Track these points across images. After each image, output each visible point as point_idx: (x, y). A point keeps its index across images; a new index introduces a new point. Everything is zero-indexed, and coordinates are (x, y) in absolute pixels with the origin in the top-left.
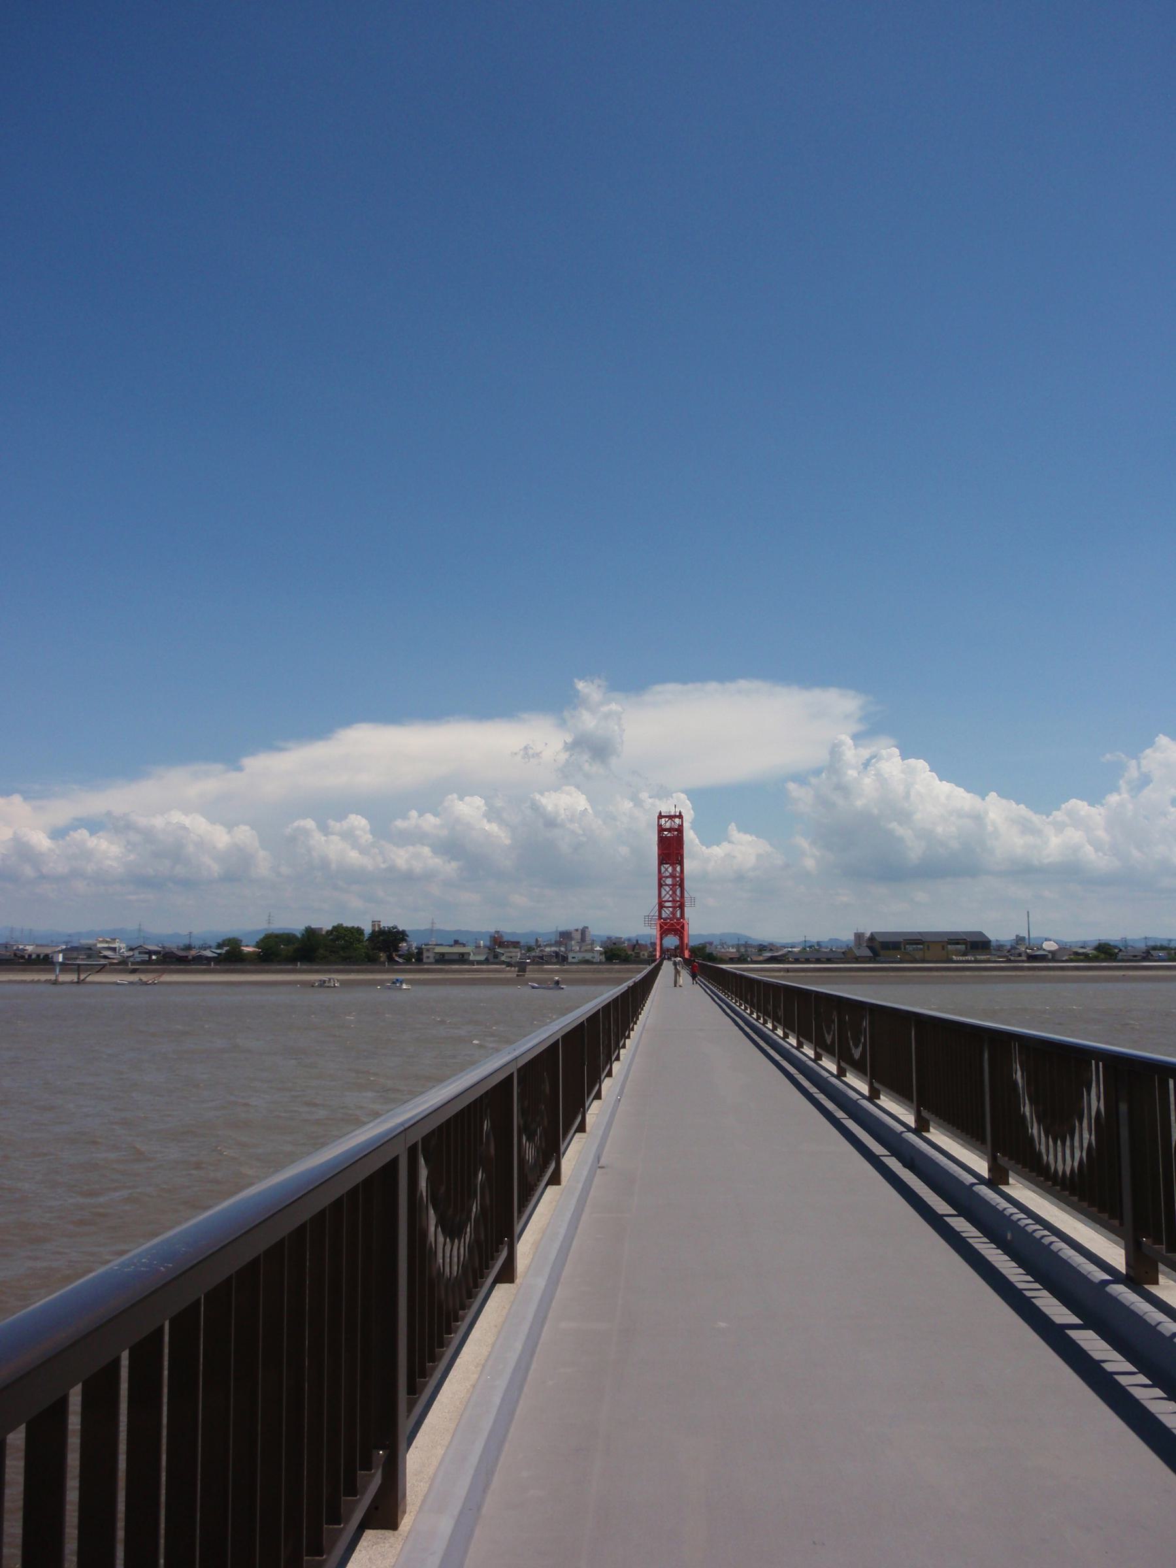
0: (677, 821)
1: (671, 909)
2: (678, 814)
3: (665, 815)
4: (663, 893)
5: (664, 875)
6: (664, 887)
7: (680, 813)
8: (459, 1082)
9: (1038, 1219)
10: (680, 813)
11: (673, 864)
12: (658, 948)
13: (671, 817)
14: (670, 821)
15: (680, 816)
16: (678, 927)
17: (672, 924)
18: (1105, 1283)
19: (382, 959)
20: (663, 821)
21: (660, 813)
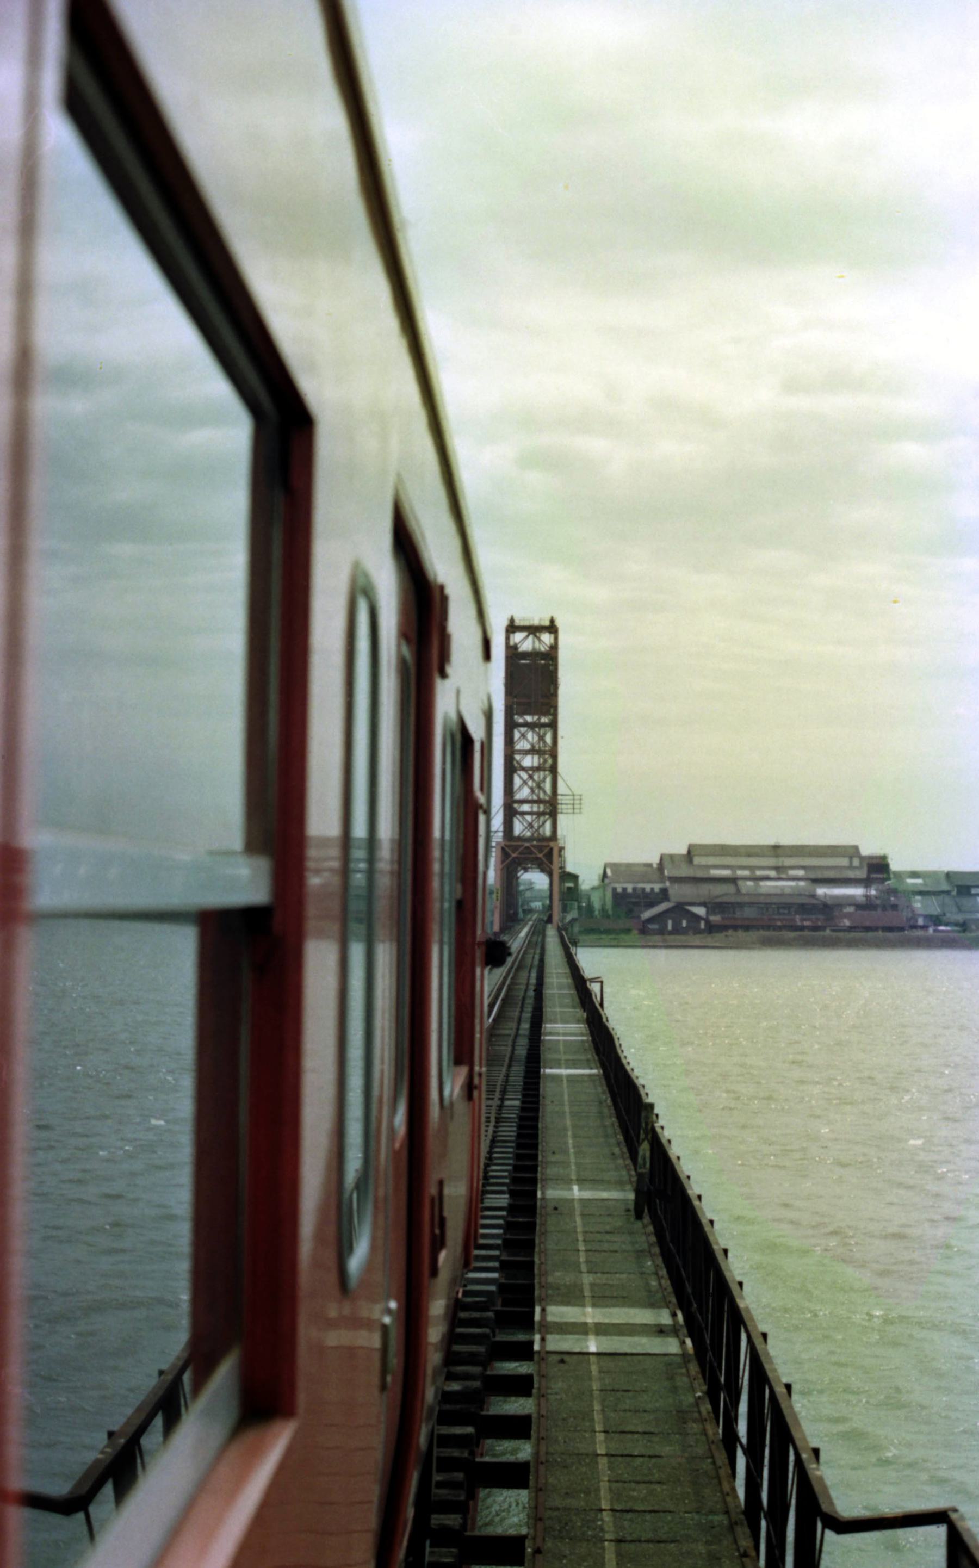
0: (547, 638)
1: (529, 818)
2: (547, 623)
3: (522, 624)
4: (517, 781)
5: (518, 747)
6: (519, 772)
7: (552, 621)
8: (435, 937)
9: (444, 763)
10: (552, 621)
11: (515, 647)
12: (936, 1157)
13: (533, 630)
14: (531, 637)
15: (552, 628)
16: (540, 856)
17: (527, 848)
18: (481, 806)
19: (775, 1023)
20: (518, 637)
21: (512, 621)
